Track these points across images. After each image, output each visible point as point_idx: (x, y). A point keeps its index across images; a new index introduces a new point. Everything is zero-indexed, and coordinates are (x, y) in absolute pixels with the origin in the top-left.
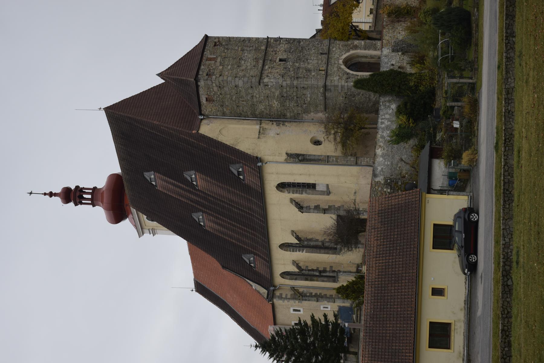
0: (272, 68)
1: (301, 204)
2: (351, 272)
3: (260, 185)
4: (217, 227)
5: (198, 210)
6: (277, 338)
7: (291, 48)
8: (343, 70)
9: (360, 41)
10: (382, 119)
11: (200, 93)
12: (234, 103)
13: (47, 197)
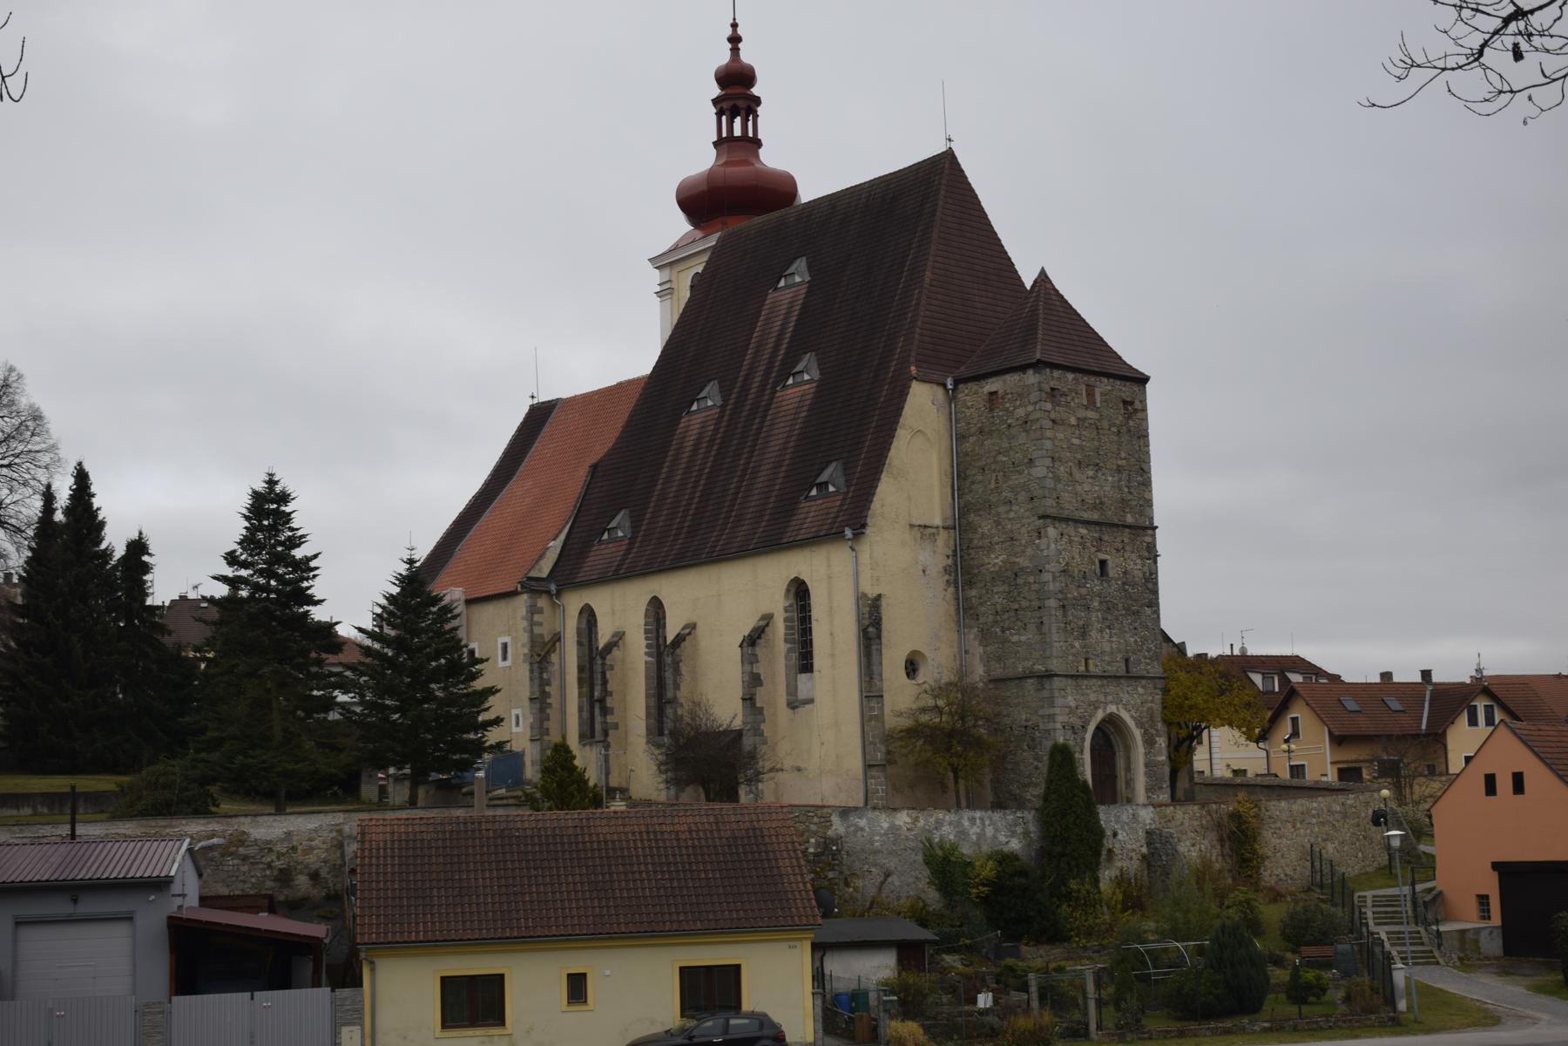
2: (607, 774)
5: (725, 393)
7: (1134, 585)
8: (1091, 716)
9: (1165, 752)
10: (982, 819)
11: (1008, 377)
13: (729, 31)
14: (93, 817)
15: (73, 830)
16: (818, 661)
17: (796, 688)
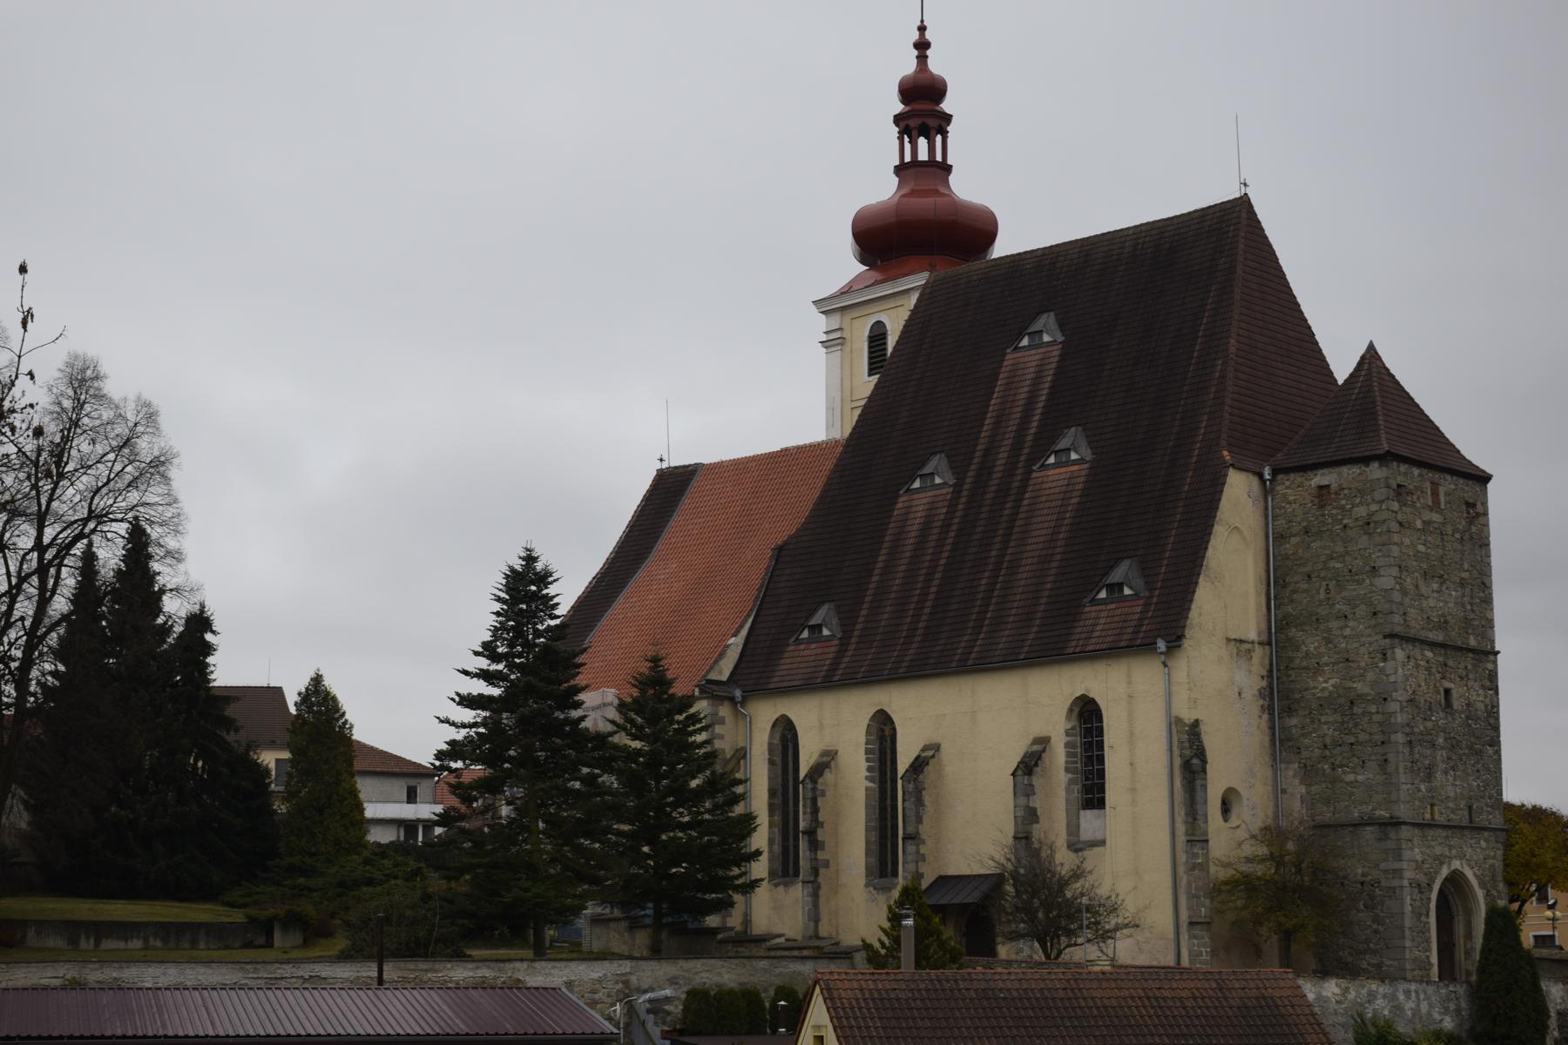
0: (1428, 669)
1: (1038, 769)
2: (817, 921)
3: (1090, 648)
4: (914, 528)
5: (959, 470)
6: (681, 718)
7: (1477, 719)
8: (1437, 872)
10: (1417, 992)
11: (1345, 470)
12: (1319, 566)
13: (916, 36)
14: (216, 954)
15: (380, 971)
16: (1111, 796)
17: (1078, 826)
